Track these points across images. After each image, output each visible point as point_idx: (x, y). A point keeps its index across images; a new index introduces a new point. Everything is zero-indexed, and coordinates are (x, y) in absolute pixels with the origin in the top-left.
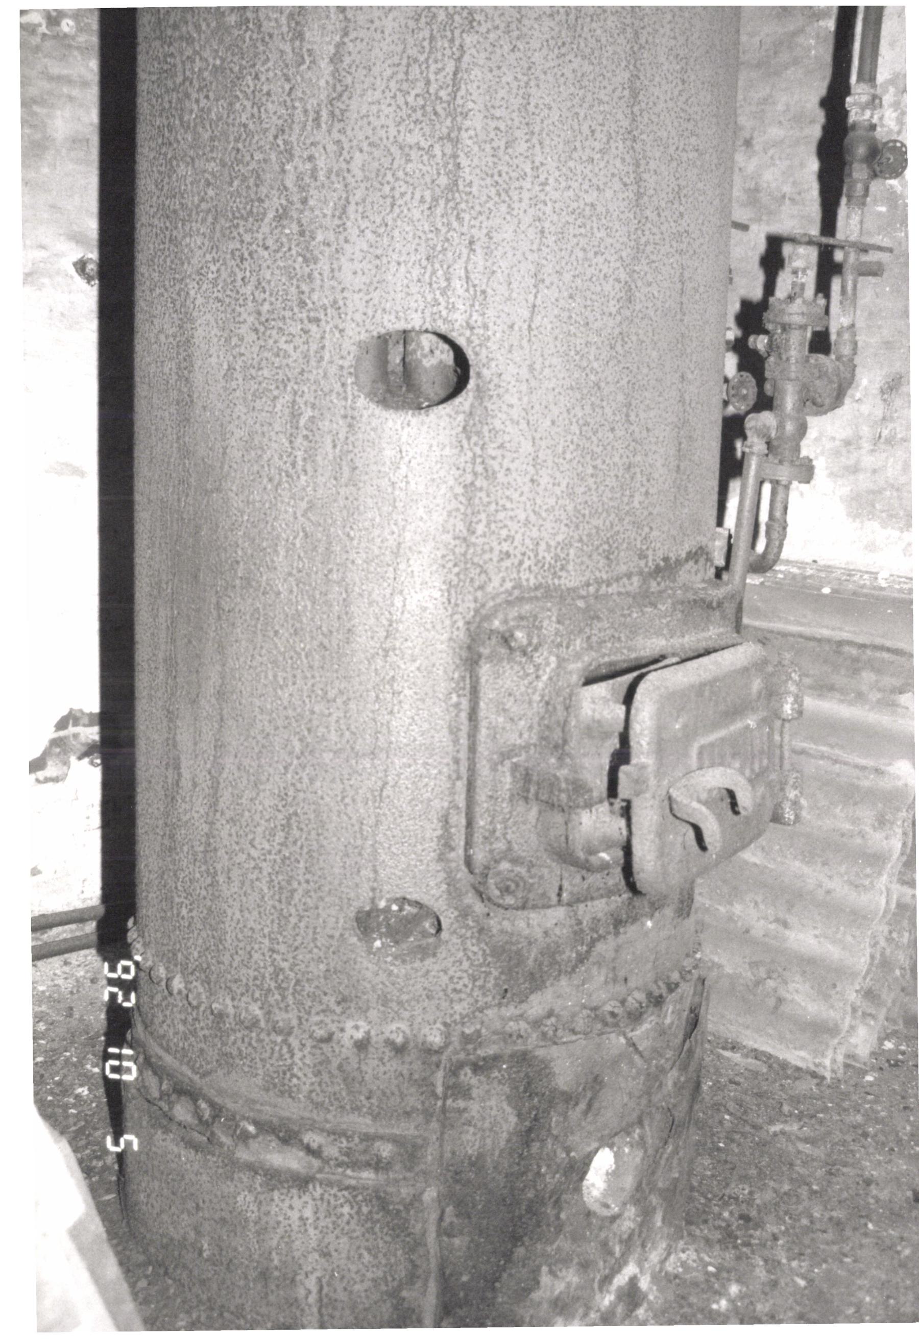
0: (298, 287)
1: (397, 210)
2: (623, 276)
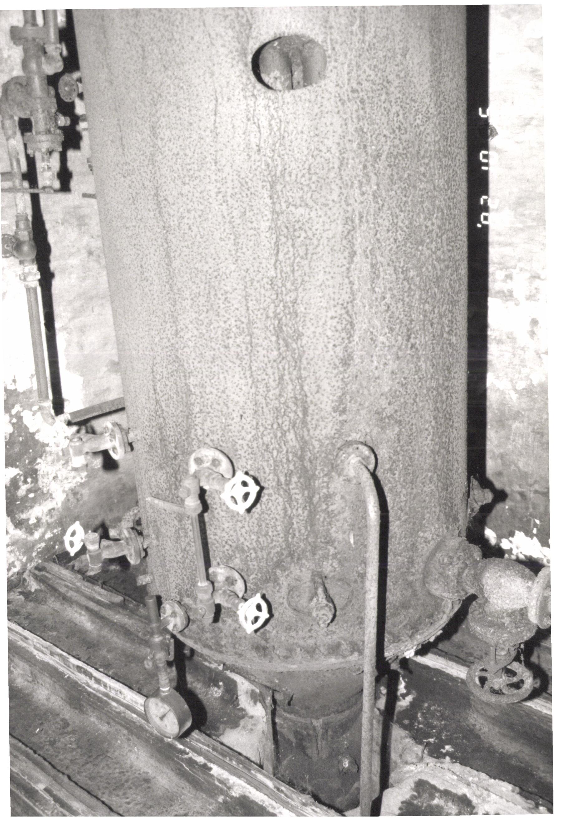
0: (365, 112)
1: (306, 166)
2: (159, 143)
